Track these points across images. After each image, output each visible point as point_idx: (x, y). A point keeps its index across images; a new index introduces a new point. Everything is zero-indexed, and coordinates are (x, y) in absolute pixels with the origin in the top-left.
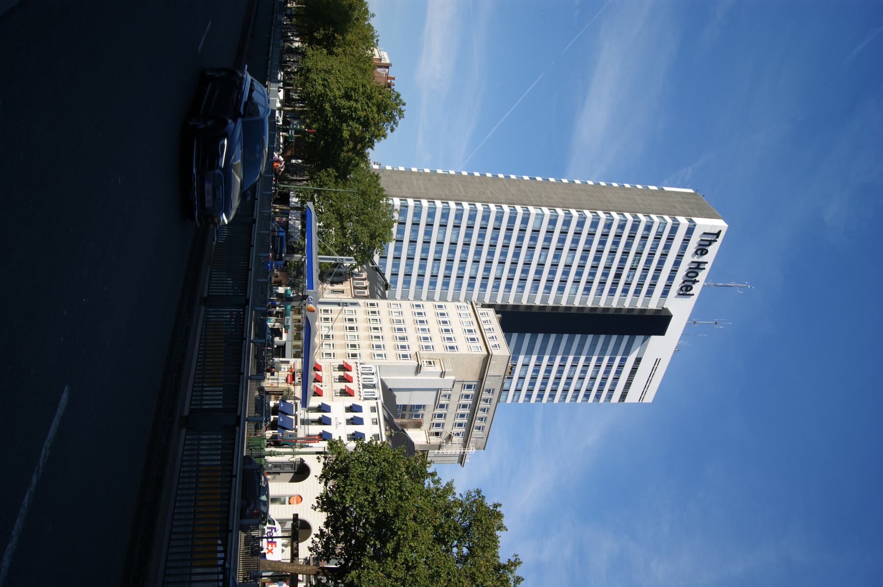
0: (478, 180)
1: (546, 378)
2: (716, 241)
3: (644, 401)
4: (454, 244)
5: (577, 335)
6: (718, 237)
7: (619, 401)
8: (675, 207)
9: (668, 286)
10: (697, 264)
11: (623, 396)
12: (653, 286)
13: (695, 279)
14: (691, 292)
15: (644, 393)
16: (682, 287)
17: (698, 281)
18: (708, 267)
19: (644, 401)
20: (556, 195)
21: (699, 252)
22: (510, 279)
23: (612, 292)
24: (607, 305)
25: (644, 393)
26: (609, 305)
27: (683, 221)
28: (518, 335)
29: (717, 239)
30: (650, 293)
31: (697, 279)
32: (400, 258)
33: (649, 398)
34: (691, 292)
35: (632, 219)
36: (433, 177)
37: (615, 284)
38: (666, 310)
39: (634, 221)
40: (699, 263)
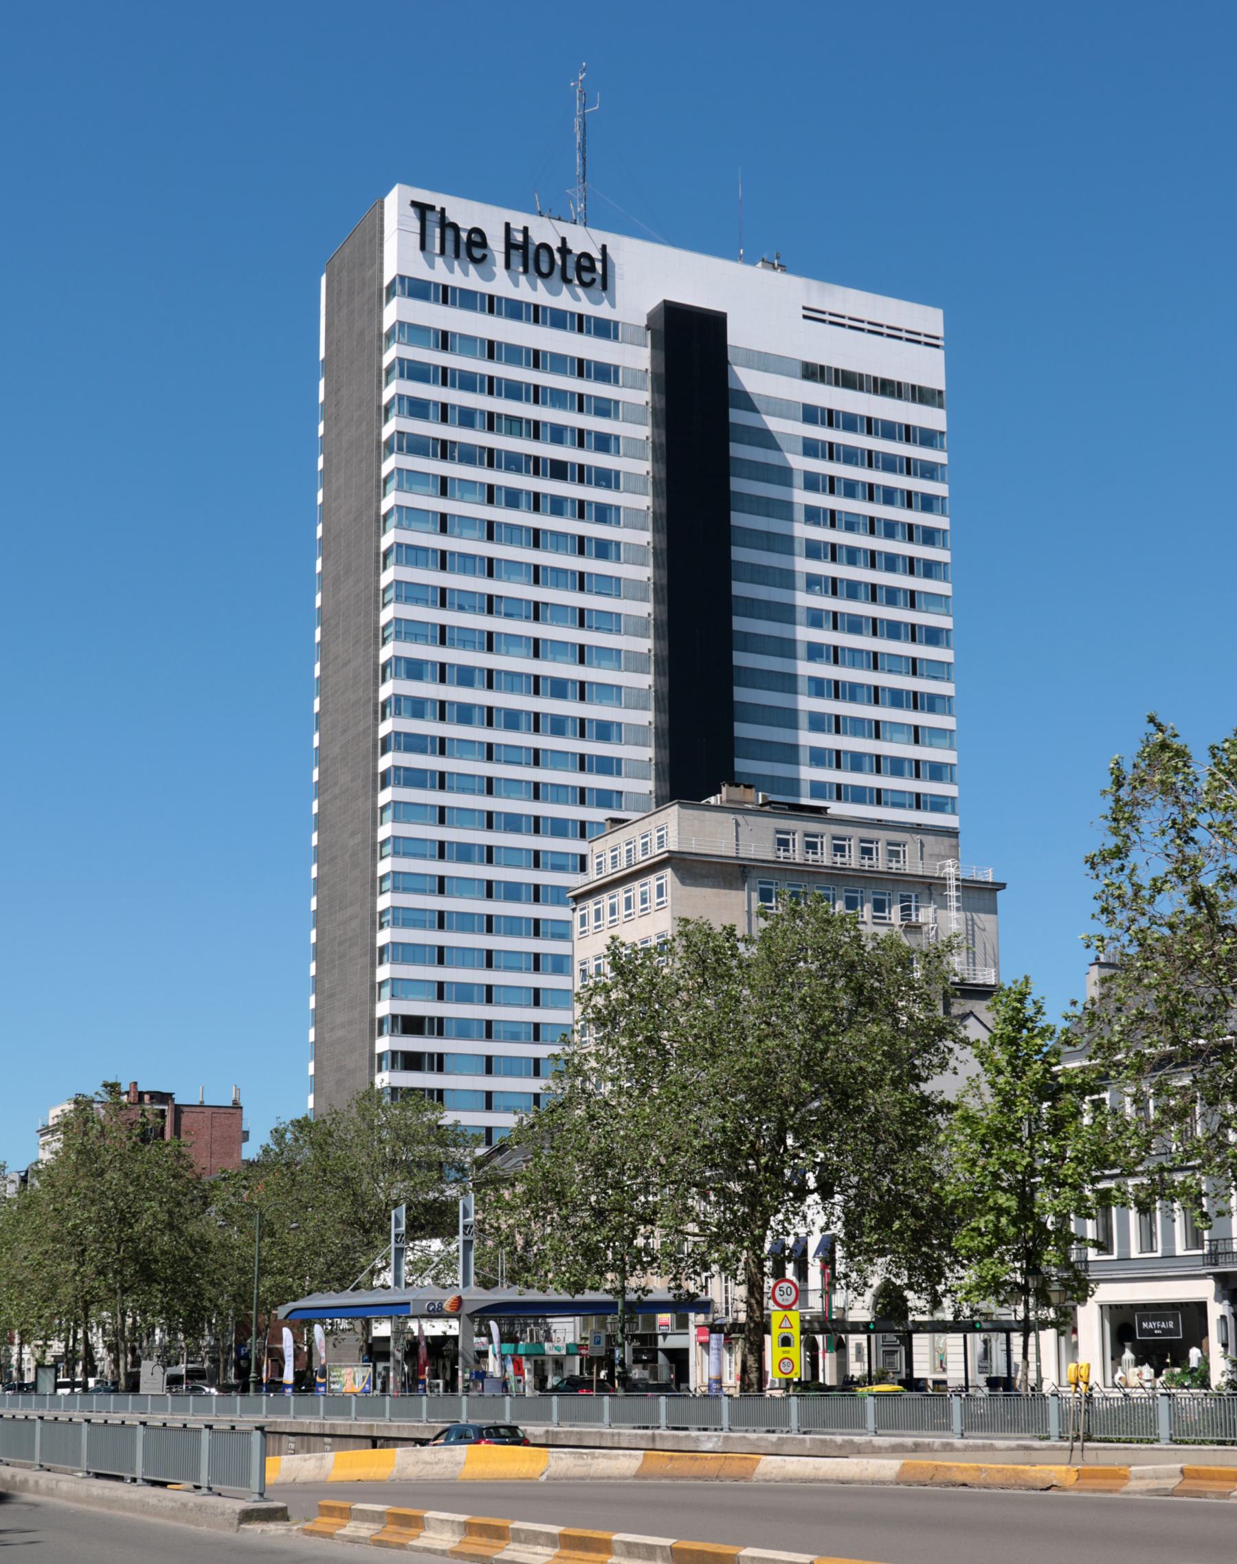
0: (326, 869)
1: (874, 593)
2: (443, 210)
3: (941, 334)
4: (491, 494)
5: (731, 420)
6: (432, 208)
7: (941, 406)
8: (362, 334)
9: (581, 324)
10: (513, 252)
11: (922, 395)
12: (581, 368)
13: (559, 250)
14: (597, 255)
15: (913, 338)
16: (584, 284)
17: (564, 240)
18: (518, 220)
19: (941, 334)
20: (349, 661)
21: (477, 253)
22: (581, 510)
23: (606, 479)
24: (646, 487)
25: (913, 338)
26: (646, 483)
27: (391, 314)
28: (738, 580)
29: (438, 209)
30: (605, 373)
31: (555, 244)
32: (537, 715)
33: (930, 320)
34: (597, 255)
35: (393, 456)
36: (327, 986)
37: (582, 474)
38: (651, 317)
39: (400, 449)
40: (510, 246)
